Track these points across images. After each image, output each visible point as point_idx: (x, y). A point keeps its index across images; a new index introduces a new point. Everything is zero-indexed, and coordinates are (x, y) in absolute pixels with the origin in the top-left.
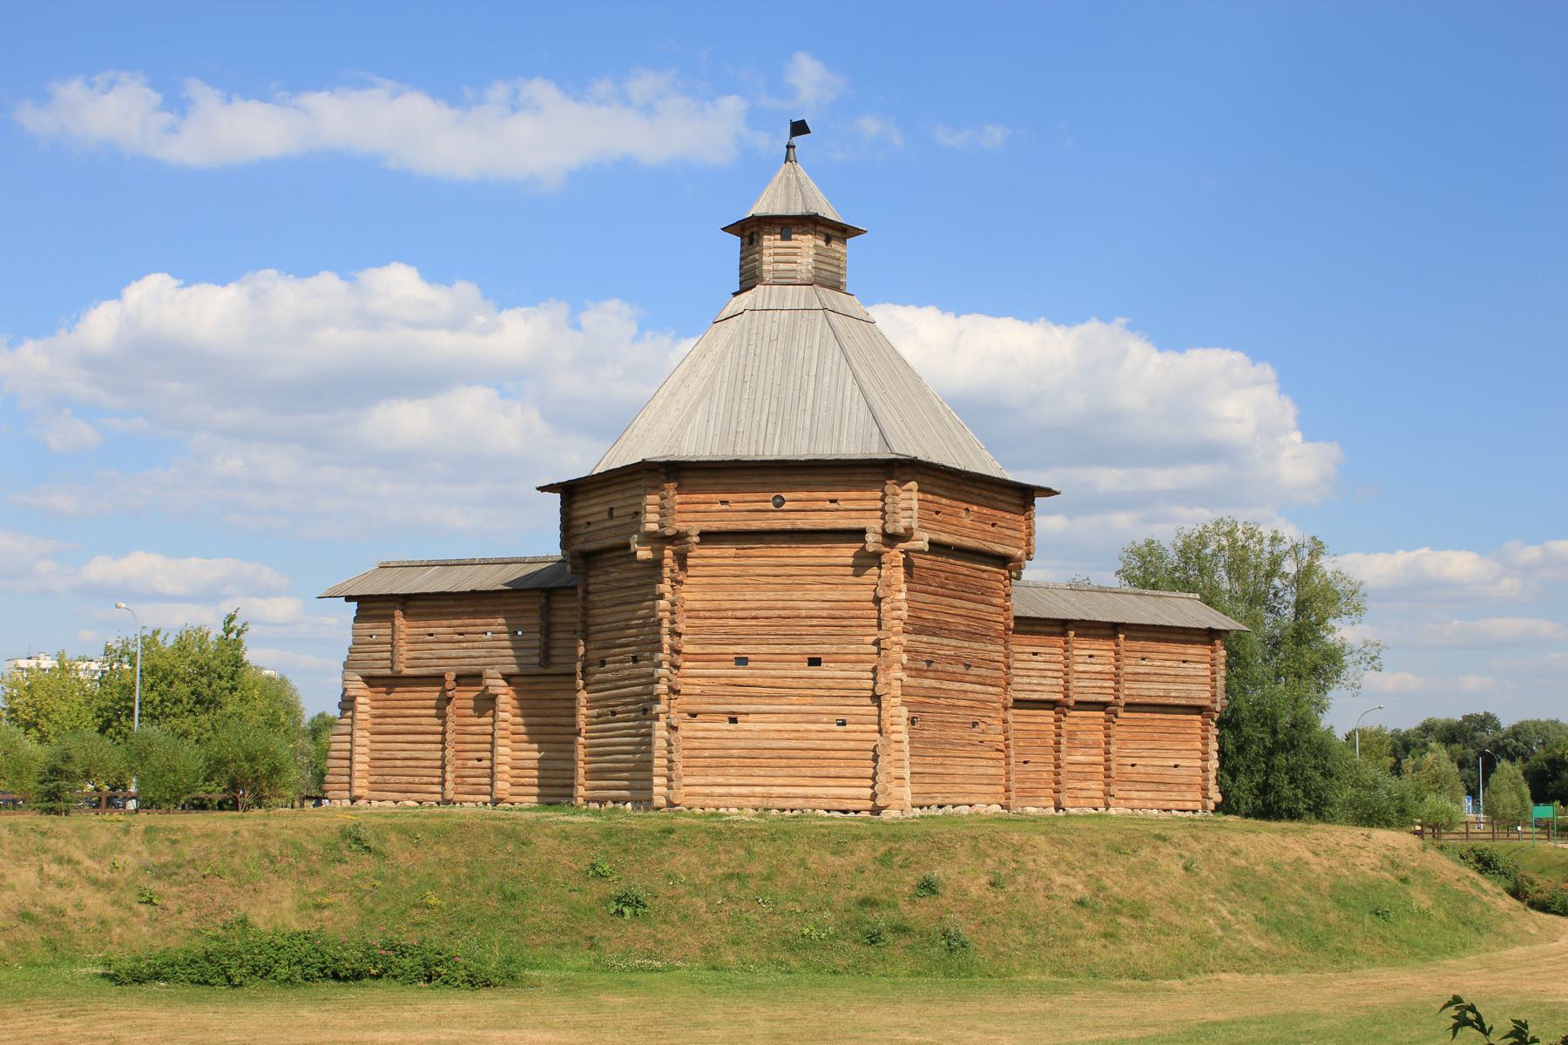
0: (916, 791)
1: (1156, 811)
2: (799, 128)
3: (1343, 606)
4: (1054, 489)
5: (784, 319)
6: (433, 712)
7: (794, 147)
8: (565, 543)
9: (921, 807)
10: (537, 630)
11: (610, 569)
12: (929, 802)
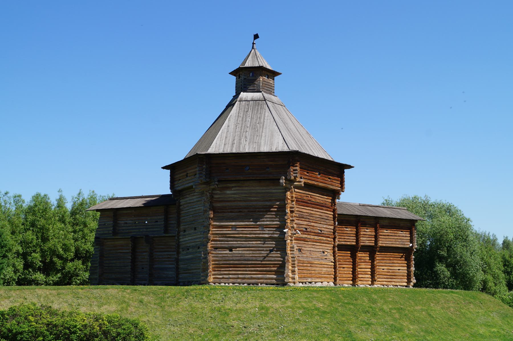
0: (300, 276)
1: (392, 286)
2: (256, 37)
3: (181, 307)
4: (352, 165)
5: (251, 104)
6: (409, 233)
7: (255, 44)
8: (172, 187)
9: (302, 283)
10: (163, 220)
11: (187, 196)
12: (305, 281)
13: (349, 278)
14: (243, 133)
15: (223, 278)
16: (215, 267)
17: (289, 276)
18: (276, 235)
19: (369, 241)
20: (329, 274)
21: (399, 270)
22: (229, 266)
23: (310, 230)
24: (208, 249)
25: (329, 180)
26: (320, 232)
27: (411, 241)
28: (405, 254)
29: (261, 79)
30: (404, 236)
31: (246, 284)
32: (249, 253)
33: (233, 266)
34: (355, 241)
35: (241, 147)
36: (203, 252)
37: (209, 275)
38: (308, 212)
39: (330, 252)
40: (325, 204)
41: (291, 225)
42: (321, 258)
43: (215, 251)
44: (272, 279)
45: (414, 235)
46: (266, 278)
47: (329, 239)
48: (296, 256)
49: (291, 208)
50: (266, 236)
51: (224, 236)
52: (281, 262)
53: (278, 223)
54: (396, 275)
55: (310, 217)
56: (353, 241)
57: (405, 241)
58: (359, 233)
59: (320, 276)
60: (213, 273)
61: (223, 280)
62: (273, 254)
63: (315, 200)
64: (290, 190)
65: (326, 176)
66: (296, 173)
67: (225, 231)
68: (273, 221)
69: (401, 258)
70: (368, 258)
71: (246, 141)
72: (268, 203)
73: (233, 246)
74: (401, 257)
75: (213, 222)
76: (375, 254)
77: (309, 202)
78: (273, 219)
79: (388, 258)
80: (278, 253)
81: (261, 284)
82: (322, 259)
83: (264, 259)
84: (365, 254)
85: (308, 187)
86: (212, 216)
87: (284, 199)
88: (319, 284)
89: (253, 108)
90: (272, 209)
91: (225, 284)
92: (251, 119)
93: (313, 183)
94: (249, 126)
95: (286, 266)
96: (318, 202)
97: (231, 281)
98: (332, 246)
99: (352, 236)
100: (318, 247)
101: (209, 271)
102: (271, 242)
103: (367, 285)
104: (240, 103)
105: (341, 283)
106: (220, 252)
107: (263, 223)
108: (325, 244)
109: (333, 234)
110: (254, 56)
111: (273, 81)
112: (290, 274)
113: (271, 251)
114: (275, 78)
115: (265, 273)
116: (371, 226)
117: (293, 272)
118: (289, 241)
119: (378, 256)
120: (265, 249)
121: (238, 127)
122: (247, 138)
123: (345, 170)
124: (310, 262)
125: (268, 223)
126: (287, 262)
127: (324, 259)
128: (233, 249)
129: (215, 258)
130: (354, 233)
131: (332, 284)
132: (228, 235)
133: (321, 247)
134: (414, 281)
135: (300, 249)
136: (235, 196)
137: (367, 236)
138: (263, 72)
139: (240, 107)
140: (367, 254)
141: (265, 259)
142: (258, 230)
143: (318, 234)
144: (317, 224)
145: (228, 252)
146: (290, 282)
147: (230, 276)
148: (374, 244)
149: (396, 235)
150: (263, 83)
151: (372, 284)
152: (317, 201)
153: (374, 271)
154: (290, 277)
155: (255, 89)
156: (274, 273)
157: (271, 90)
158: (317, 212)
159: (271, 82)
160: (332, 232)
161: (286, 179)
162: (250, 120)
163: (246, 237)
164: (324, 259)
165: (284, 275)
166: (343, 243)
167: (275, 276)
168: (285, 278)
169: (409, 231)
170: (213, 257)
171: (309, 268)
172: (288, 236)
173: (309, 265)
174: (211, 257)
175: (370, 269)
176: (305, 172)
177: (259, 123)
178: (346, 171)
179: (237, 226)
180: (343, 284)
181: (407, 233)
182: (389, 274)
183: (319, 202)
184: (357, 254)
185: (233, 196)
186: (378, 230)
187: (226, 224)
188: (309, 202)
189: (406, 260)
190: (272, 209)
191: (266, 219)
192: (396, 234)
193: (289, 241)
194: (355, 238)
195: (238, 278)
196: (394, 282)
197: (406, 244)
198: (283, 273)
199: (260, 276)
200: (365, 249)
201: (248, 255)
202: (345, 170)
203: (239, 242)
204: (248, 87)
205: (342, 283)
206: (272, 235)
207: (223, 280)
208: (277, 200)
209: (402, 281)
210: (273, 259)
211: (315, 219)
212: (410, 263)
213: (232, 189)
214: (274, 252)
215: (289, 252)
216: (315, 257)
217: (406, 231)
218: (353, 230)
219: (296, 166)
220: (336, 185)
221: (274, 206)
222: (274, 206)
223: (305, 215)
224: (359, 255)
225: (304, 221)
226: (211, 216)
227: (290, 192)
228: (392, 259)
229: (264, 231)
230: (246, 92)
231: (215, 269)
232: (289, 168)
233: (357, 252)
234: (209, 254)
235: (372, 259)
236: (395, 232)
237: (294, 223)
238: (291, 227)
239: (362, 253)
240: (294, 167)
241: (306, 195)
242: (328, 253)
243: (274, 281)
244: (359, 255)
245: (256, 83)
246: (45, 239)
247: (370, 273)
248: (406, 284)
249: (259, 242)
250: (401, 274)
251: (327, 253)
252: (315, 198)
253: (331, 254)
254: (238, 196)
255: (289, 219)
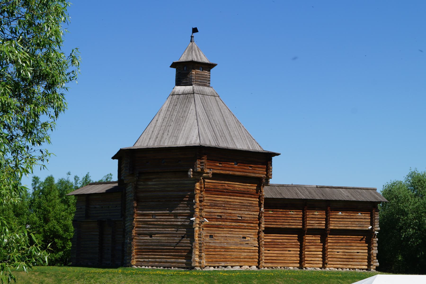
2: (195, 30)
6: (369, 215)
7: (193, 37)
9: (214, 267)
13: (295, 261)
14: (167, 127)
15: (144, 261)
16: (138, 252)
17: (195, 261)
18: (187, 223)
19: (318, 225)
20: (251, 258)
21: (358, 253)
22: (149, 250)
23: (226, 217)
24: (132, 235)
25: (251, 168)
26: (240, 218)
27: (372, 223)
28: (365, 237)
29: (194, 73)
30: (363, 218)
31: (162, 267)
32: (165, 239)
33: (152, 251)
34: (301, 224)
35: (162, 141)
36: (128, 238)
37: (132, 258)
38: (223, 200)
39: (254, 237)
40: (248, 191)
41: (200, 214)
42: (240, 243)
43: (138, 237)
44: (182, 263)
45: (374, 218)
46: (178, 262)
47: (252, 225)
48: (204, 242)
49: (200, 197)
50: (179, 223)
51: (145, 224)
52: (190, 248)
53: (189, 211)
54: (353, 258)
55: (226, 205)
56: (299, 224)
57: (364, 223)
58: (305, 217)
59: (239, 261)
60: (136, 256)
61: (143, 263)
62: (184, 240)
63: (232, 188)
64: (199, 181)
65: (246, 165)
66: (203, 166)
67: (147, 219)
68: (185, 210)
69: (360, 240)
70: (320, 241)
71: (168, 134)
72: (181, 193)
73: (152, 233)
74: (361, 239)
75: (137, 211)
76: (326, 237)
77: (225, 191)
78: (185, 208)
79: (344, 241)
80: (188, 239)
81: (174, 268)
82: (242, 244)
83: (177, 244)
84: (315, 237)
85: (215, 176)
86: (136, 205)
87: (193, 189)
88: (237, 268)
89: (181, 103)
90: (185, 199)
91: (145, 267)
92: (177, 113)
93: (226, 173)
94: (173, 120)
95: (193, 251)
96: (237, 190)
97: (150, 264)
98: (257, 231)
99: (298, 219)
100: (237, 233)
101: (132, 255)
102: (183, 229)
103: (316, 268)
104: (172, 97)
105: (286, 266)
106: (142, 238)
107: (176, 211)
108: (247, 230)
109: (258, 220)
110: (190, 49)
111: (208, 72)
112: (197, 259)
113: (183, 237)
114: (212, 70)
115: (178, 257)
116: (320, 209)
117: (200, 257)
118: (197, 228)
119: (330, 239)
120: (178, 236)
121: (164, 121)
122: (169, 132)
123: (272, 158)
124: (224, 247)
125: (181, 211)
126: (194, 248)
127: (245, 244)
128: (153, 236)
129: (138, 244)
130: (300, 217)
131: (254, 268)
132: (149, 223)
133: (241, 233)
134: (376, 263)
135: (213, 235)
136: (156, 186)
137: (316, 219)
138: (196, 65)
139: (171, 102)
140: (318, 237)
141: (178, 245)
142: (172, 218)
143: (236, 221)
144: (236, 211)
145: (148, 238)
146: (197, 266)
147: (150, 260)
148: (324, 227)
149: (352, 217)
150: (195, 76)
151: (324, 267)
152: (236, 189)
153: (325, 254)
154: (197, 262)
155: (187, 83)
156: (184, 257)
157: (206, 82)
158: (245, 200)
159: (206, 74)
160: (257, 218)
161: (193, 171)
162: (176, 114)
163: (154, 224)
164: (245, 244)
165: (191, 260)
166: (287, 226)
167: (184, 261)
168: (192, 262)
169: (370, 213)
170: (137, 242)
171: (223, 253)
172: (196, 224)
173: (223, 250)
174: (134, 242)
175: (322, 252)
176: (218, 163)
177: (182, 117)
178: (274, 159)
179: (156, 215)
180: (288, 267)
181: (367, 215)
182: (344, 257)
183: (239, 190)
184: (304, 237)
185: (153, 186)
186: (329, 213)
187: (148, 212)
188: (225, 191)
189: (366, 243)
190: (185, 199)
191: (180, 208)
192: (352, 217)
193: (197, 228)
194: (302, 221)
195: (156, 262)
196: (351, 265)
197: (366, 226)
198: (191, 258)
199: (173, 260)
200: (314, 232)
201: (164, 241)
202: (272, 158)
203: (157, 229)
204: (181, 80)
205: (287, 266)
206: (184, 223)
207: (143, 263)
208: (189, 191)
209: (362, 264)
210: (184, 245)
211: (233, 207)
212: (371, 245)
213: (153, 180)
214: (185, 239)
215: (197, 239)
216: (232, 242)
217: (366, 213)
218: (299, 213)
219: (203, 159)
220: (260, 173)
221: (187, 196)
222: (187, 196)
223: (219, 203)
224: (306, 238)
225: (217, 209)
226: (135, 205)
227: (200, 183)
228: (349, 242)
229: (178, 219)
230: (180, 86)
231: (138, 253)
232: (196, 161)
233: (304, 235)
234: (133, 239)
235: (324, 241)
236: (351, 215)
237: (203, 211)
238: (199, 215)
239: (312, 236)
240: (201, 160)
241: (221, 184)
242: (251, 238)
243: (184, 265)
244: (308, 238)
245: (188, 76)
246: (46, 221)
247: (321, 256)
248: (366, 267)
249: (174, 229)
250: (360, 257)
251: (249, 238)
252: (234, 186)
253: (255, 239)
254: (157, 187)
255: (198, 208)
